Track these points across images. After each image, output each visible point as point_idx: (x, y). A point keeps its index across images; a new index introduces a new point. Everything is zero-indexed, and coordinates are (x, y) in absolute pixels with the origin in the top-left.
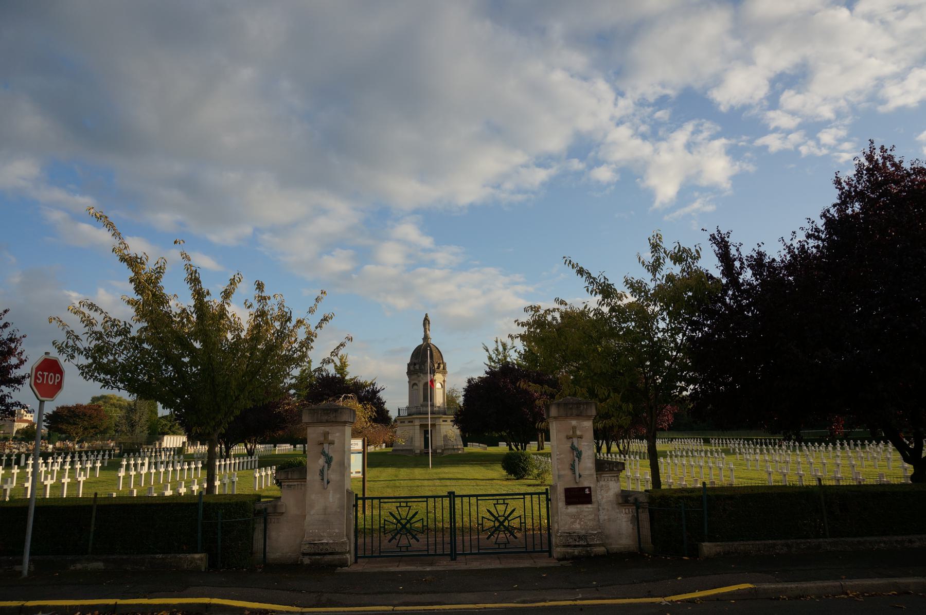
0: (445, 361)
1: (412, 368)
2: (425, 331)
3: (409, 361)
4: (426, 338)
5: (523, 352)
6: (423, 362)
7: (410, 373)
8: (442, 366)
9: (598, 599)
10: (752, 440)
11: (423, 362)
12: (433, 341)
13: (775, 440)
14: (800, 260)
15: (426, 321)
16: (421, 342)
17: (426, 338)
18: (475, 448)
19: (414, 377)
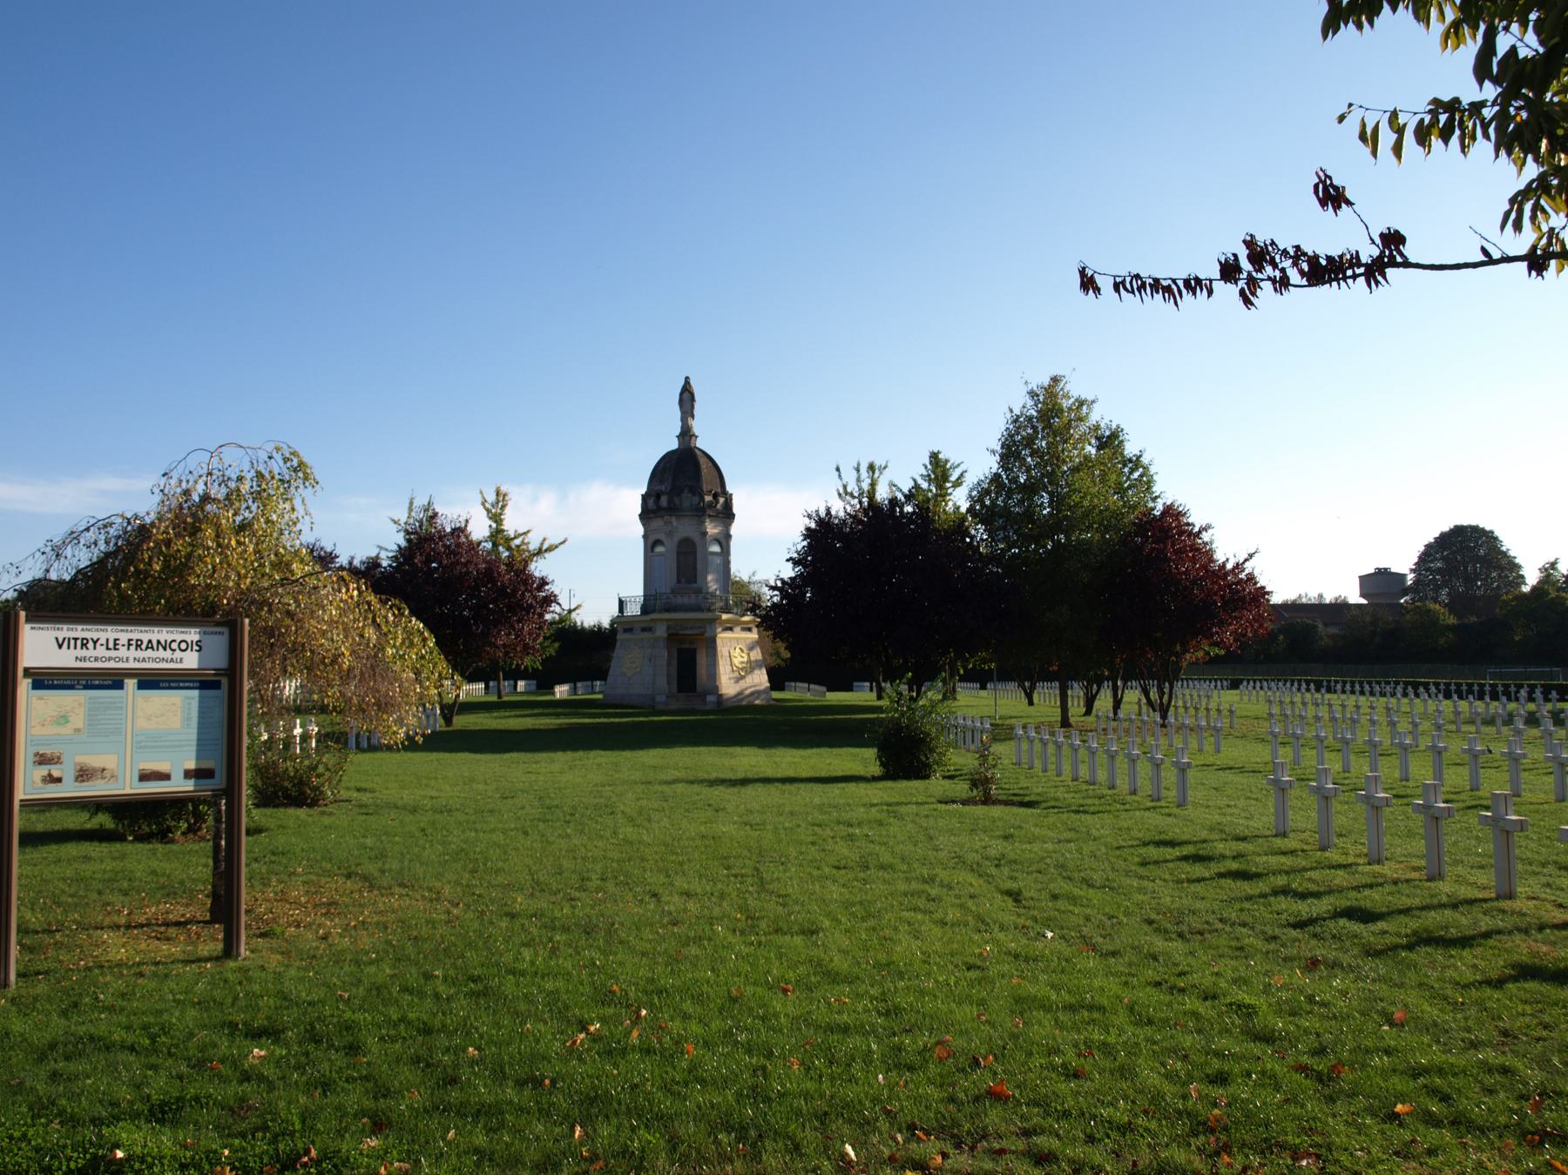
0: (729, 489)
1: (651, 502)
2: (684, 420)
3: (644, 490)
4: (686, 434)
5: (882, 494)
6: (685, 492)
7: (645, 516)
8: (722, 500)
9: (600, 715)
10: (1426, 686)
11: (685, 492)
12: (700, 444)
13: (1353, 683)
14: (583, 629)
15: (687, 398)
16: (674, 445)
17: (686, 434)
18: (800, 694)
19: (657, 523)
